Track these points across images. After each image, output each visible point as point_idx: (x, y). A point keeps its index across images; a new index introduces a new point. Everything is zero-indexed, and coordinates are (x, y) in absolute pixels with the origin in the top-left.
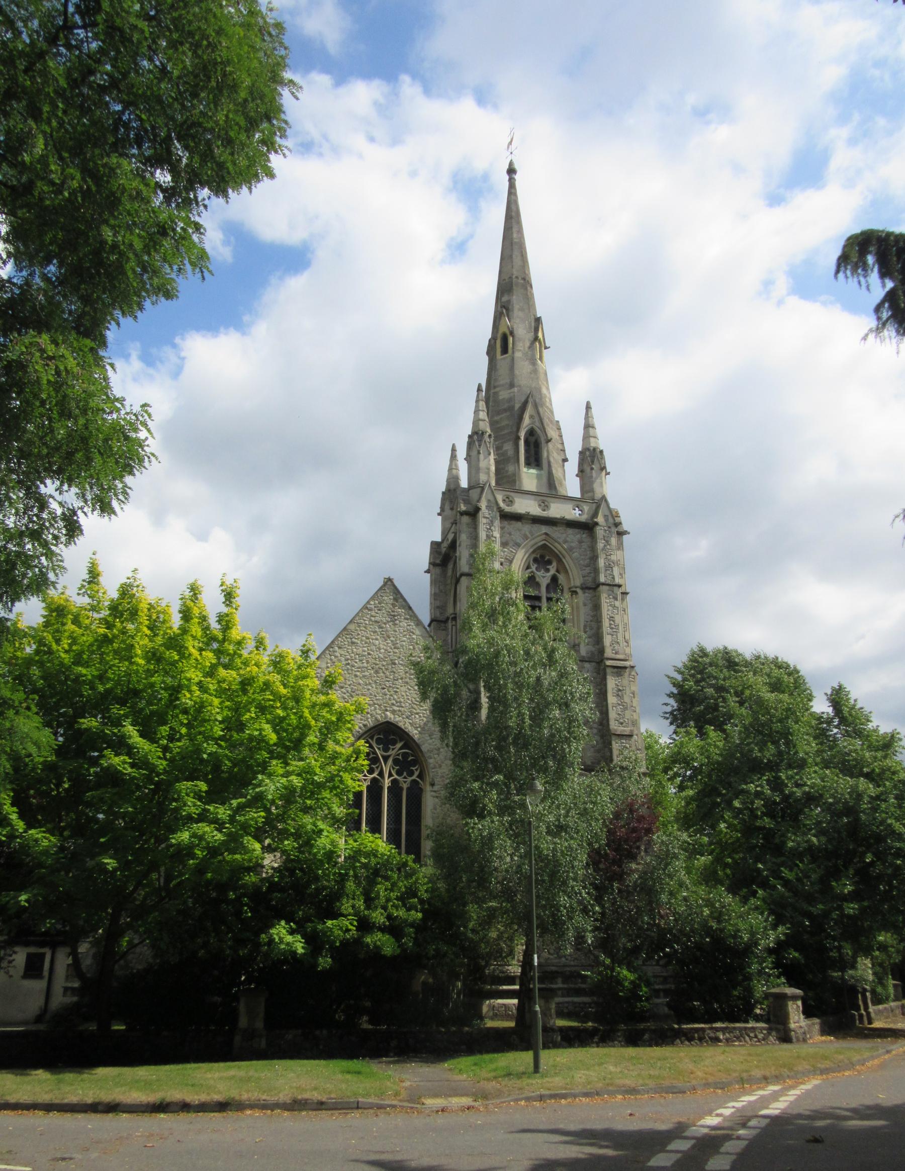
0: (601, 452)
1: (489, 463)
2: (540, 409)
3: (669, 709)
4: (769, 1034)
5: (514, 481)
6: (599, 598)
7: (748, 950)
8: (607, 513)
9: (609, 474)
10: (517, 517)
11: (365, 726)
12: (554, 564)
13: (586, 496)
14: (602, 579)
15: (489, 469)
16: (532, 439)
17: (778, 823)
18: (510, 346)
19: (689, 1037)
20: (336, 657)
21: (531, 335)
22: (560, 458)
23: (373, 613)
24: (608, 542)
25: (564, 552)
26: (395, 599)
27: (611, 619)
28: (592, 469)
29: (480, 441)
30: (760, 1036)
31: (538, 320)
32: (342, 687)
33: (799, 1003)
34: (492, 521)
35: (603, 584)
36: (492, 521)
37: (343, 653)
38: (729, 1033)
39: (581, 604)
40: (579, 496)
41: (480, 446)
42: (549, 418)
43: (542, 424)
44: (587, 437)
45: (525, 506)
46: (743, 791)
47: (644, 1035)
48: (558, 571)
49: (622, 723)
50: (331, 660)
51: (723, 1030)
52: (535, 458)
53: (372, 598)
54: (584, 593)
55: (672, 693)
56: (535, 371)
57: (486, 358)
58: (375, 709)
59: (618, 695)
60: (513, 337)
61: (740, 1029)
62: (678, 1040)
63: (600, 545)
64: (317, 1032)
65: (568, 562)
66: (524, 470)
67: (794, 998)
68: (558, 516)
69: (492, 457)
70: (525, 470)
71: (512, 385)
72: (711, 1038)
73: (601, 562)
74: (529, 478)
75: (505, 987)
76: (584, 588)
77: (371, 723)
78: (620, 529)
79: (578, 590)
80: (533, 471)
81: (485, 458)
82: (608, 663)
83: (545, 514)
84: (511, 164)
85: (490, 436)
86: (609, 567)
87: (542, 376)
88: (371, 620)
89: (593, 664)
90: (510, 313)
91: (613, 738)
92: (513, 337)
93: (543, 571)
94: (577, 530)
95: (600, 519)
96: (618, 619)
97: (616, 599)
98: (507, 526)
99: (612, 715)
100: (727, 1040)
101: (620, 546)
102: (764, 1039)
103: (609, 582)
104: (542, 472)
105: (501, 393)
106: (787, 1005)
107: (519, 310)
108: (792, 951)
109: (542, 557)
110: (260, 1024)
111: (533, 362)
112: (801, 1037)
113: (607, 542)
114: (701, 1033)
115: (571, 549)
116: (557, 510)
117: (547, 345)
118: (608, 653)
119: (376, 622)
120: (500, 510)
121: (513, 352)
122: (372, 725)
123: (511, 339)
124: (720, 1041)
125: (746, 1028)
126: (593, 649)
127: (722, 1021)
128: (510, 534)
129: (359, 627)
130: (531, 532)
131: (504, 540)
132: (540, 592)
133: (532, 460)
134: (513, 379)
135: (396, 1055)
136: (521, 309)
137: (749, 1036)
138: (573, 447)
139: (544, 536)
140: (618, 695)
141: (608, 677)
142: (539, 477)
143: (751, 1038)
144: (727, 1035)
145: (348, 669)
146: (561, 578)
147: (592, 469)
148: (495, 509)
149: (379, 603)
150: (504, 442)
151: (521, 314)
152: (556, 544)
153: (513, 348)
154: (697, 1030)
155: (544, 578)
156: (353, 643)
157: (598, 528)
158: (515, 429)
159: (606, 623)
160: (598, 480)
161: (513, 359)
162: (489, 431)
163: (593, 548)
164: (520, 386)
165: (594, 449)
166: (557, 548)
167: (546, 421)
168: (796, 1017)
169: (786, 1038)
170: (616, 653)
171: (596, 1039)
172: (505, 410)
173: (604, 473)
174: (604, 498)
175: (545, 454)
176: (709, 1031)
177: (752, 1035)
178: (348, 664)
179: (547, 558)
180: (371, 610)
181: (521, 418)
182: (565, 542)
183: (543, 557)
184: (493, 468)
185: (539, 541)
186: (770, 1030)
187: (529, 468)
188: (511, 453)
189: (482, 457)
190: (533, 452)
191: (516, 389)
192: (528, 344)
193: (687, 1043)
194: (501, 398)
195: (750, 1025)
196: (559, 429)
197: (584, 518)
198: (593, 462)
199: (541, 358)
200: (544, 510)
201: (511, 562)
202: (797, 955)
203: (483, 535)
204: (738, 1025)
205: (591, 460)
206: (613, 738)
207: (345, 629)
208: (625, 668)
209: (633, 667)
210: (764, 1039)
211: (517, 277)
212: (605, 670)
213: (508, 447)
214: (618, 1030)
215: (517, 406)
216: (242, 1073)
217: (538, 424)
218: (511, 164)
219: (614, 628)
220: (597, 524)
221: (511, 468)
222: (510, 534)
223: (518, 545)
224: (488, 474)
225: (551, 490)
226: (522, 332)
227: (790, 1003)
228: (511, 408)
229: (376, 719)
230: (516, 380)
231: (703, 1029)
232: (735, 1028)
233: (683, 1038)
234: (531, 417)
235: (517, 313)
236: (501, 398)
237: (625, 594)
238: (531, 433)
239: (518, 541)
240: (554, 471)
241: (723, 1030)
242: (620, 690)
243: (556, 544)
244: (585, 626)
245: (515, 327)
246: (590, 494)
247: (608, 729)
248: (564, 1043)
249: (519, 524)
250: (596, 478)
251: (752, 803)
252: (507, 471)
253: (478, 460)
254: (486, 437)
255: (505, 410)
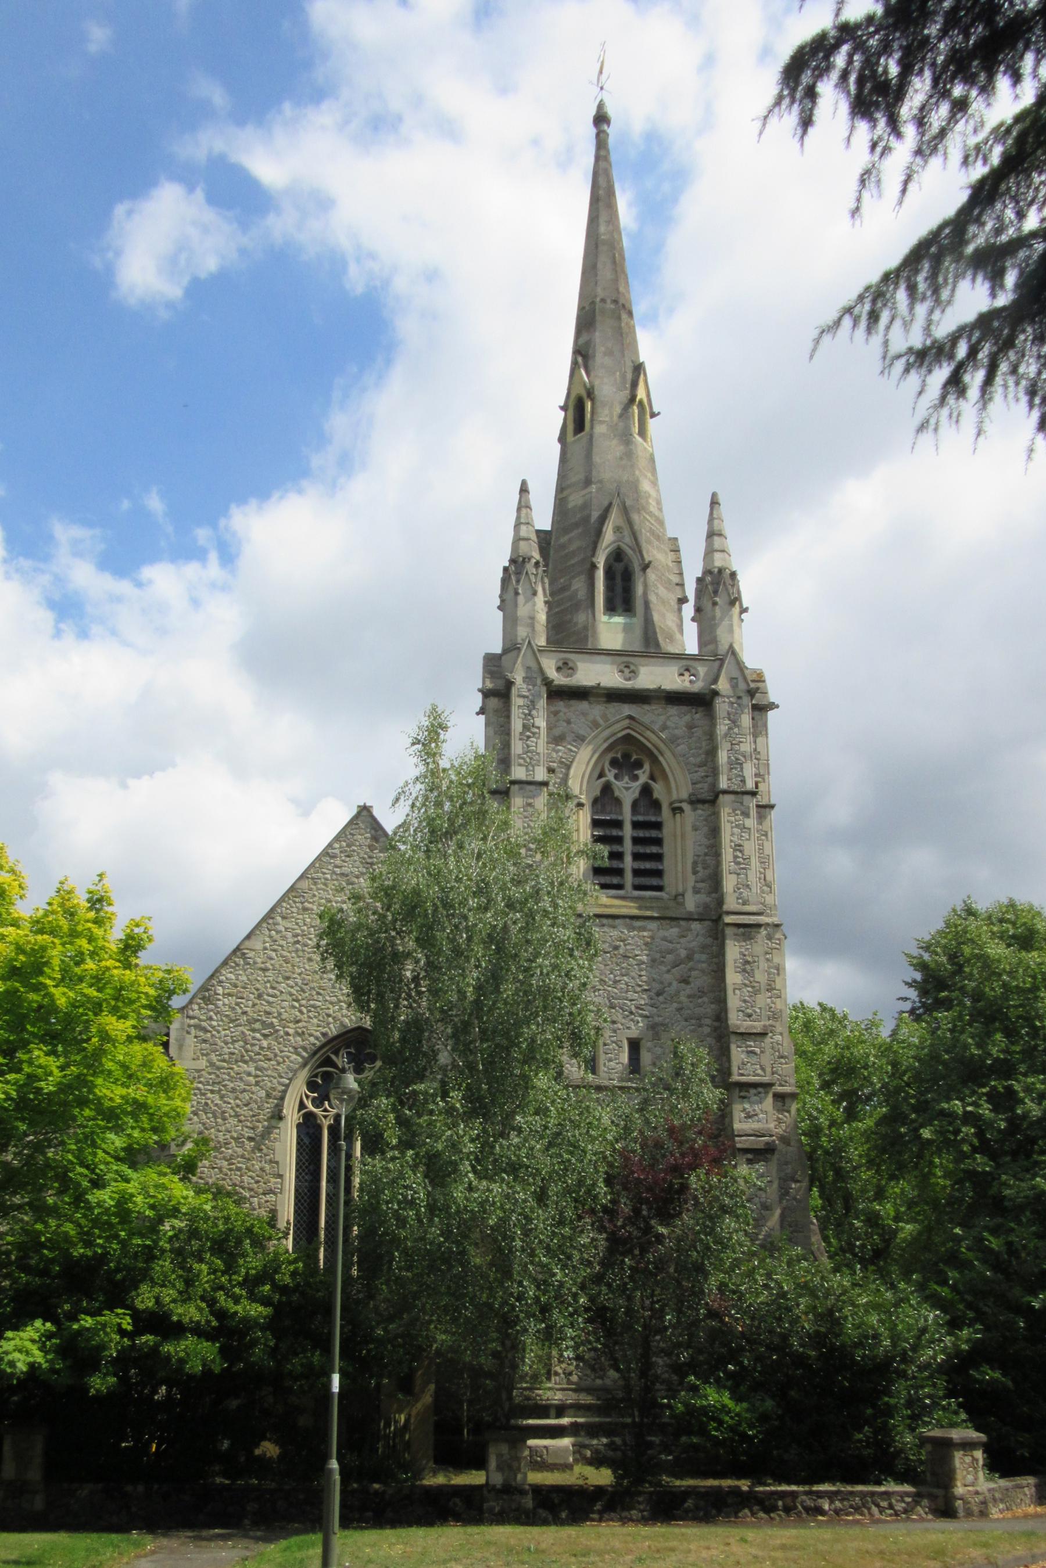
0: (733, 575)
1: (539, 608)
2: (635, 517)
3: (908, 1006)
4: (917, 1503)
5: (586, 638)
6: (716, 815)
7: (882, 1371)
8: (736, 674)
9: (746, 610)
10: (580, 694)
11: (324, 1035)
12: (647, 766)
13: (705, 650)
14: (723, 784)
15: (532, 618)
16: (619, 567)
17: (998, 1166)
18: (588, 416)
19: (766, 1505)
20: (278, 932)
21: (627, 393)
22: (672, 598)
23: (338, 862)
24: (735, 723)
25: (662, 746)
26: (375, 838)
27: (738, 848)
28: (715, 604)
29: (518, 573)
30: (900, 1506)
31: (638, 369)
32: (288, 978)
33: (979, 1454)
34: (532, 702)
35: (725, 792)
36: (532, 702)
37: (289, 925)
38: (842, 1500)
39: (689, 828)
40: (696, 652)
41: (518, 581)
42: (652, 532)
43: (636, 539)
44: (710, 552)
45: (594, 673)
46: (943, 1113)
47: (684, 1501)
48: (652, 777)
49: (750, 1016)
50: (270, 937)
51: (831, 1496)
52: (623, 594)
53: (337, 839)
54: (695, 810)
55: (915, 981)
56: (629, 454)
57: (559, 446)
58: (341, 1009)
59: (744, 970)
60: (593, 400)
61: (863, 1495)
62: (746, 1511)
63: (722, 728)
64: (129, 1488)
65: (668, 761)
66: (603, 618)
67: (967, 1446)
68: (652, 686)
69: (540, 599)
70: (604, 618)
71: (588, 482)
72: (807, 1509)
73: (723, 757)
74: (611, 630)
75: (531, 1422)
76: (695, 801)
77: (333, 1030)
78: (758, 699)
79: (686, 806)
80: (618, 620)
81: (526, 602)
82: (728, 919)
83: (629, 685)
84: (601, 106)
85: (537, 564)
86: (736, 764)
87: (642, 463)
88: (334, 873)
89: (707, 923)
90: (590, 363)
91: (733, 1038)
92: (593, 400)
93: (626, 779)
94: (684, 708)
95: (723, 685)
96: (750, 848)
97: (746, 814)
98: (564, 710)
99: (733, 1002)
100: (837, 1512)
101: (759, 729)
102: (905, 1511)
103: (735, 788)
104: (634, 620)
105: (571, 498)
106: (952, 1457)
107: (605, 354)
108: (985, 1368)
109: (626, 756)
110: (34, 1475)
111: (626, 438)
112: (976, 1509)
113: (734, 722)
114: (788, 1500)
115: (673, 740)
116: (654, 676)
117: (656, 410)
118: (731, 903)
119: (342, 874)
120: (547, 683)
121: (592, 428)
122: (335, 1033)
123: (589, 405)
124: (822, 1513)
125: (873, 1494)
126: (708, 900)
127: (832, 1480)
128: (569, 722)
129: (315, 884)
130: (605, 717)
131: (557, 732)
132: (621, 814)
133: (618, 601)
134: (590, 471)
135: (256, 1524)
136: (609, 353)
137: (878, 1506)
138: (693, 570)
139: (627, 722)
140: (744, 970)
141: (727, 942)
142: (627, 629)
143: (882, 1510)
144: (838, 1504)
145: (297, 951)
146: (658, 790)
147: (715, 604)
148: (539, 681)
149: (348, 846)
150: (573, 577)
151: (607, 361)
152: (648, 734)
153: (592, 420)
154: (783, 1495)
155: (627, 791)
156: (305, 909)
157: (718, 701)
158: (589, 554)
159: (727, 855)
160: (726, 623)
161: (591, 437)
162: (536, 556)
163: (711, 736)
164: (601, 482)
165: (721, 571)
166: (650, 739)
167: (644, 535)
168: (970, 1478)
169: (946, 1510)
170: (744, 904)
171: (598, 1507)
172: (576, 525)
173: (736, 609)
174: (732, 651)
175: (639, 590)
176: (804, 1497)
177: (884, 1504)
178: (298, 942)
179: (634, 757)
180: (334, 857)
181: (599, 533)
182: (664, 728)
183: (627, 755)
184: (542, 617)
185: (619, 729)
186: (918, 1497)
187: (611, 616)
188: (582, 594)
189: (521, 599)
190: (619, 589)
191: (593, 488)
192: (618, 410)
193: (762, 1514)
194: (570, 505)
195: (883, 1489)
196: (677, 551)
197: (698, 687)
198: (716, 592)
199: (643, 432)
200: (629, 679)
201: (568, 767)
202: (997, 1375)
203: (517, 725)
204: (860, 1488)
205: (718, 588)
206: (733, 1038)
207: (292, 889)
208: (759, 926)
209: (777, 926)
210: (905, 1511)
211: (603, 300)
212: (723, 931)
213: (579, 585)
214: (640, 1493)
215: (595, 515)
216: (833, 1489)
217: (628, 539)
218: (601, 106)
219: (742, 863)
220: (716, 693)
221: (581, 618)
222: (569, 722)
223: (581, 739)
224: (532, 626)
225: (650, 645)
226: (609, 391)
227: (958, 1455)
228: (586, 519)
229: (342, 1024)
230: (594, 473)
231: (794, 1495)
232: (852, 1493)
233: (756, 1508)
234: (617, 529)
235: (600, 359)
236: (570, 505)
237: (765, 808)
238: (617, 555)
239: (582, 732)
240: (656, 617)
241: (831, 1496)
242: (747, 962)
243: (648, 734)
244: (695, 864)
245: (597, 383)
246: (711, 647)
247: (727, 1026)
248: (543, 1513)
249: (584, 705)
250: (722, 619)
251: (957, 1132)
252: (576, 624)
253: (516, 605)
254: (530, 567)
255: (576, 525)
